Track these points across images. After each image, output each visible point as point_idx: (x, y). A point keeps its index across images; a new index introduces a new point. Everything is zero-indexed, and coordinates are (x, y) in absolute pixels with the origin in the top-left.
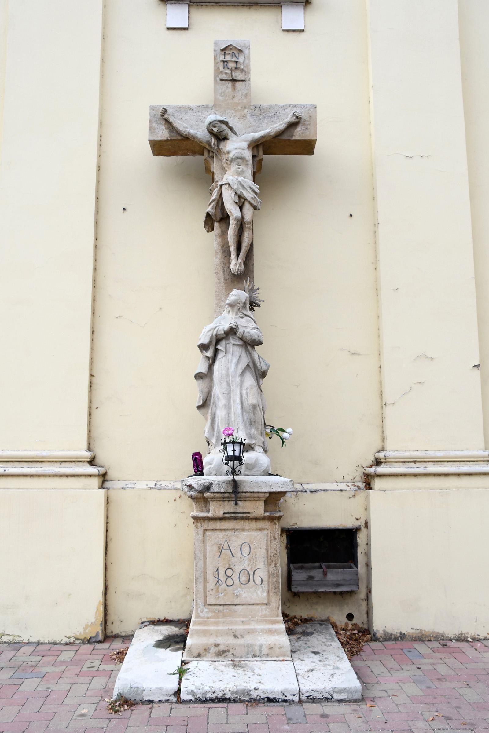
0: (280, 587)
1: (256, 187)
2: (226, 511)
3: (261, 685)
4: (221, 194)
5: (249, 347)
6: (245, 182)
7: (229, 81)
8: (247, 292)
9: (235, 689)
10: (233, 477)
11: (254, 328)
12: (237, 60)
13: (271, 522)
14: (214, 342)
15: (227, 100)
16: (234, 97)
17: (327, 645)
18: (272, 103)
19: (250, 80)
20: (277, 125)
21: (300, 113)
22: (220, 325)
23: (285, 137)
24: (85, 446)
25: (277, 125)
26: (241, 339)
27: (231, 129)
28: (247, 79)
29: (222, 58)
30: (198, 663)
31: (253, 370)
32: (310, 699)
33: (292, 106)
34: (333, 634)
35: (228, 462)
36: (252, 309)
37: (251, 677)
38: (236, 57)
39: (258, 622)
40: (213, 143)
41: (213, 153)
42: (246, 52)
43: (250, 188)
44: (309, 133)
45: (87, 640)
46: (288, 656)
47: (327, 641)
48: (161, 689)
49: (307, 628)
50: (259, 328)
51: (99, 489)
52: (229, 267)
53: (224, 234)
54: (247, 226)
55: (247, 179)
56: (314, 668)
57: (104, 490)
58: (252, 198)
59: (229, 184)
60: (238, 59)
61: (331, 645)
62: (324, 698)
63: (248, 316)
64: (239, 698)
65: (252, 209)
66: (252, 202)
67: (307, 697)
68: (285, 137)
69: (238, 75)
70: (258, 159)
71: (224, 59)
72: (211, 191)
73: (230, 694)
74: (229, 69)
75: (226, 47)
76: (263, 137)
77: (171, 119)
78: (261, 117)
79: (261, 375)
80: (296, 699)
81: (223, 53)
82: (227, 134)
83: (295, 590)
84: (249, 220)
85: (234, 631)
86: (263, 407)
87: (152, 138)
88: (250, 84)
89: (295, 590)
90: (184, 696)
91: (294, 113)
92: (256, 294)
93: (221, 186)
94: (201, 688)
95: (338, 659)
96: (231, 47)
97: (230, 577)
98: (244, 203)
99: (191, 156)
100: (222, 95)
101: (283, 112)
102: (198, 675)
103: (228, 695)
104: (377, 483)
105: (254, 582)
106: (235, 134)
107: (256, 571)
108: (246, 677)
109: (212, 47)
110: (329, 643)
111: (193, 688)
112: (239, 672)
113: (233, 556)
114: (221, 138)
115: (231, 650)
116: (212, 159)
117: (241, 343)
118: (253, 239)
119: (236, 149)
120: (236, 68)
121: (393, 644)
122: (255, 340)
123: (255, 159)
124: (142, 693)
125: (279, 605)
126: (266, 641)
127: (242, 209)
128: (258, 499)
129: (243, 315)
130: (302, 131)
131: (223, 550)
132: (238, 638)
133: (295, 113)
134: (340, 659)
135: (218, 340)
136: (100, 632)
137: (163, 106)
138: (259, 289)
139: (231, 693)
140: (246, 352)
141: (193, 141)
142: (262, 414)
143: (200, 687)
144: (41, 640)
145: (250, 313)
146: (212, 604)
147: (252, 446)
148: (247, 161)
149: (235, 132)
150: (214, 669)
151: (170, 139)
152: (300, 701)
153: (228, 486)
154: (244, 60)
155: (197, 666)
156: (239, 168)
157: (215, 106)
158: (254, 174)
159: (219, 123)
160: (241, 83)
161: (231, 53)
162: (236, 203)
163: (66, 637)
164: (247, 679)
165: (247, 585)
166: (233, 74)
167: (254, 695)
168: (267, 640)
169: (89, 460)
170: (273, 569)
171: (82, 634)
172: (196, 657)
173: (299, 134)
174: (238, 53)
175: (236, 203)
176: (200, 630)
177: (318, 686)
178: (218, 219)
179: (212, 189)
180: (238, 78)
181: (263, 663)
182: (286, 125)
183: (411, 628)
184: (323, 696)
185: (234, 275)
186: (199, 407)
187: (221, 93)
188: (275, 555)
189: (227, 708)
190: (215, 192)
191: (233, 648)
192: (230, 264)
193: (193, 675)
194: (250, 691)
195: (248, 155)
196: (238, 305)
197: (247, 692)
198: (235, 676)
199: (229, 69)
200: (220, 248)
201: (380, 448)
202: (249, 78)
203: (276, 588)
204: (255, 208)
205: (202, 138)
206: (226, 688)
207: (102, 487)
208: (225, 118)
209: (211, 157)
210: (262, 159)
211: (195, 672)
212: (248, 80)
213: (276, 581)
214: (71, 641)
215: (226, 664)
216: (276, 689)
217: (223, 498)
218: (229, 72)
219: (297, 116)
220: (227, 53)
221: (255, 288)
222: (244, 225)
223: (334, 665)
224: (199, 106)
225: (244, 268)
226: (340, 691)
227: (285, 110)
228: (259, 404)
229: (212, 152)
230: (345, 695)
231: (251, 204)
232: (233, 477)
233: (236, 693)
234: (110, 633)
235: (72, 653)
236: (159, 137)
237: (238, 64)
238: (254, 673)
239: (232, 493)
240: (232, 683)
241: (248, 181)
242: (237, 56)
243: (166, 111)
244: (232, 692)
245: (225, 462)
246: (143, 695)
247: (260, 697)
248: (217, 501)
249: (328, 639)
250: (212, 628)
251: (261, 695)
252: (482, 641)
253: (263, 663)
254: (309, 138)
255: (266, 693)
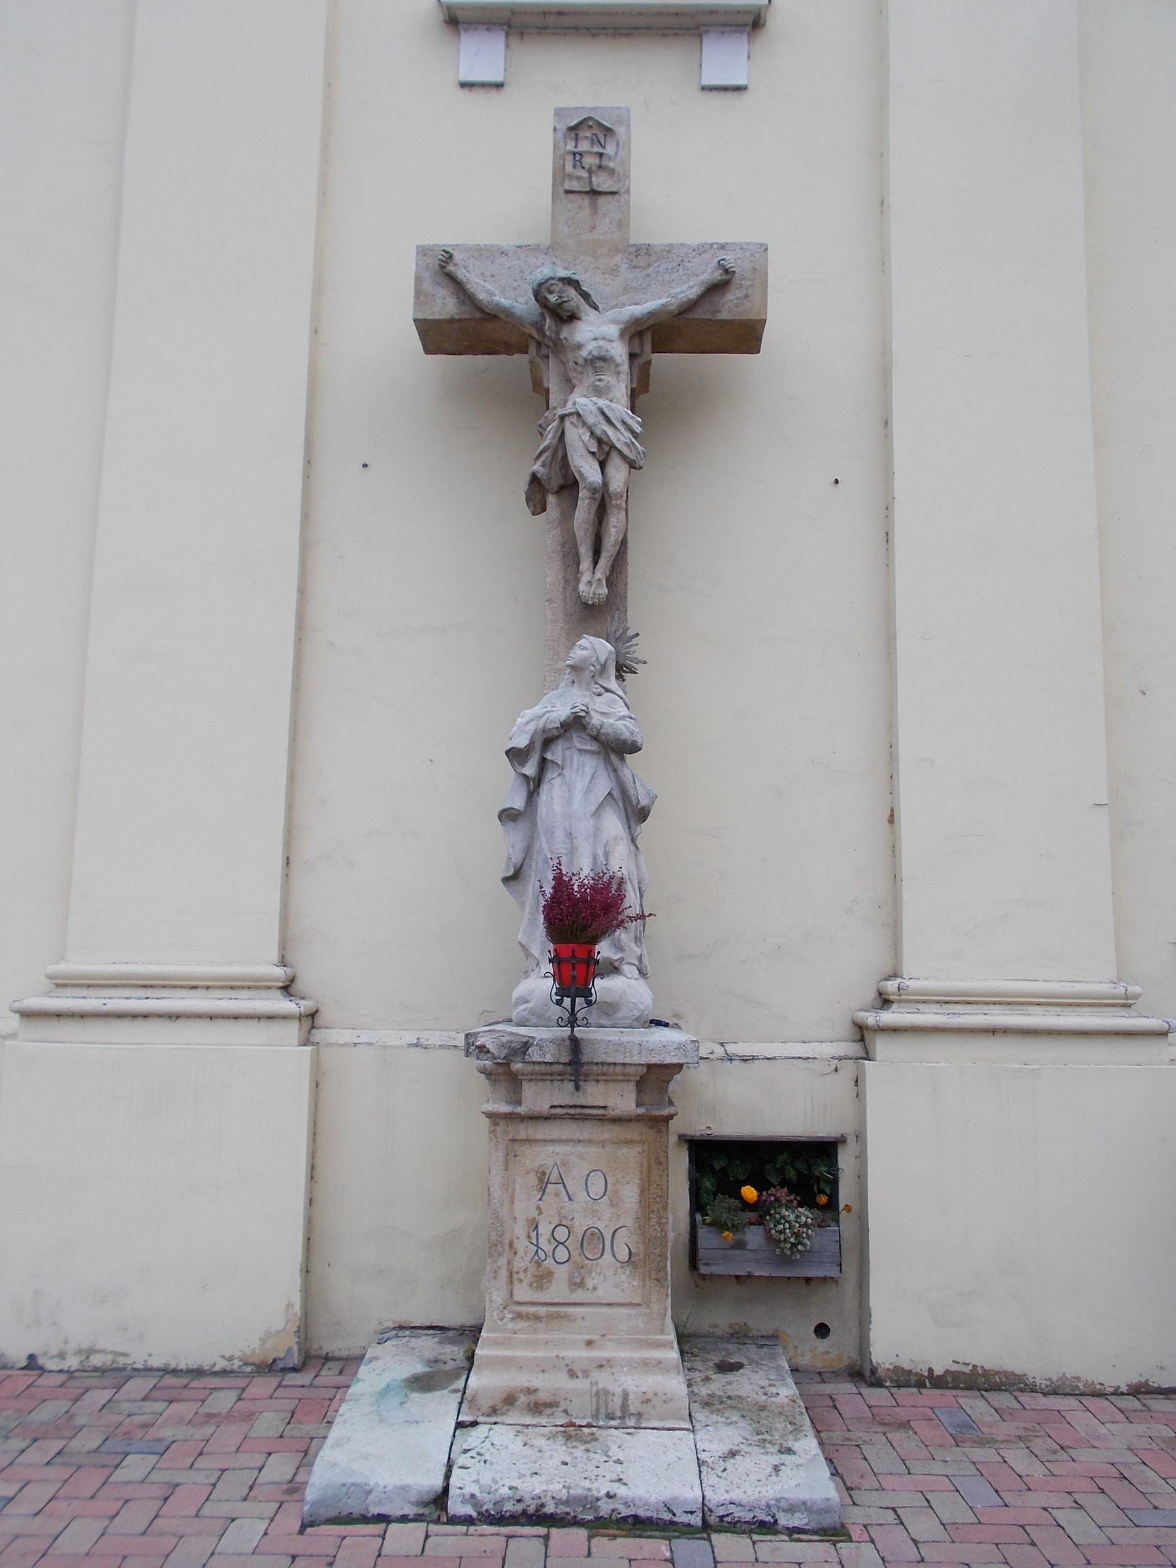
0: (669, 1268)
1: (635, 422)
2: (556, 1103)
3: (622, 1487)
4: (563, 434)
5: (613, 757)
6: (613, 410)
7: (583, 195)
8: (613, 642)
9: (564, 1494)
10: (572, 1031)
11: (623, 718)
12: (601, 150)
13: (652, 1127)
14: (538, 746)
15: (580, 234)
16: (593, 228)
17: (769, 1394)
18: (674, 241)
19: (628, 191)
20: (684, 287)
21: (732, 261)
22: (554, 709)
23: (701, 313)
24: (274, 956)
25: (684, 287)
26: (596, 738)
27: (585, 296)
28: (623, 190)
29: (570, 146)
30: (489, 1430)
31: (621, 806)
32: (727, 1522)
33: (715, 246)
34: (783, 1368)
35: (562, 1000)
36: (620, 677)
37: (602, 1466)
38: (601, 145)
39: (619, 1343)
40: (547, 327)
41: (548, 347)
42: (620, 131)
43: (624, 423)
44: (750, 305)
45: (268, 1365)
46: (684, 1420)
47: (770, 1385)
48: (404, 1489)
49: (730, 1354)
50: (633, 716)
51: (301, 1045)
52: (576, 589)
53: (567, 516)
54: (613, 502)
55: (617, 403)
56: (737, 1448)
57: (310, 1048)
58: (626, 443)
59: (578, 415)
60: (604, 148)
61: (778, 1394)
62: (757, 1521)
63: (613, 692)
64: (572, 1514)
65: (624, 468)
66: (626, 451)
67: (719, 1517)
68: (701, 313)
69: (602, 182)
70: (641, 360)
71: (576, 147)
72: (540, 429)
73: (554, 1506)
74: (583, 168)
75: (580, 123)
76: (651, 314)
77: (461, 274)
78: (649, 272)
79: (636, 814)
80: (696, 1520)
81: (573, 135)
82: (578, 308)
83: (704, 1270)
84: (619, 490)
85: (569, 1362)
86: (639, 883)
87: (420, 316)
88: (628, 201)
89: (704, 1270)
90: (456, 1507)
91: (719, 262)
92: (631, 646)
93: (562, 418)
94: (493, 1489)
95: (790, 1428)
96: (590, 123)
97: (562, 1243)
98: (608, 453)
99: (505, 356)
100: (570, 222)
101: (698, 261)
102: (487, 1457)
103: (550, 1509)
104: (882, 1046)
105: (614, 1256)
106: (595, 307)
107: (618, 1231)
108: (591, 1467)
109: (549, 121)
110: (773, 1390)
111: (475, 1489)
112: (575, 1455)
113: (570, 1199)
114: (565, 317)
115: (562, 1402)
116: (546, 360)
117: (594, 747)
118: (627, 529)
119: (596, 339)
120: (600, 167)
121: (912, 1394)
122: (625, 742)
123: (635, 362)
124: (366, 1499)
125: (666, 1310)
126: (637, 1387)
127: (605, 468)
128: (626, 1078)
129: (600, 689)
130: (735, 301)
131: (549, 1185)
132: (577, 1377)
133: (721, 262)
134: (794, 1430)
135: (548, 740)
136: (295, 1348)
137: (444, 245)
138: (637, 635)
139: (556, 1504)
140: (606, 766)
141: (505, 322)
142: (637, 898)
143: (491, 1487)
144: (171, 1362)
145: (617, 686)
146: (522, 1301)
147: (616, 964)
148: (617, 365)
149: (594, 303)
150: (525, 1445)
151: (458, 317)
152: (706, 1526)
153: (560, 1050)
154: (617, 151)
155: (487, 1437)
156: (600, 380)
157: (552, 250)
158: (634, 395)
159: (560, 284)
160: (610, 197)
161: (589, 135)
162: (593, 453)
163: (223, 1357)
164: (591, 1472)
165: (599, 1261)
166: (594, 179)
167: (605, 1508)
168: (638, 1384)
169: (281, 984)
170: (653, 1228)
171: (257, 1352)
172: (488, 1416)
173: (730, 307)
174: (605, 135)
175: (593, 453)
176: (498, 1357)
177: (745, 1492)
178: (556, 488)
179: (544, 425)
180: (604, 188)
181: (628, 1434)
182: (702, 288)
183: (954, 1361)
184: (754, 1518)
185: (586, 605)
186: (506, 880)
187: (568, 219)
188: (658, 1199)
189: (546, 1538)
190: (550, 431)
191: (565, 1399)
192: (578, 581)
193: (478, 1457)
194: (598, 1499)
195: (619, 351)
196: (592, 668)
197: (590, 1502)
198: (566, 1464)
199: (583, 168)
200: (559, 548)
201: (888, 971)
202: (627, 187)
203: (659, 1271)
204: (632, 465)
205: (525, 315)
206: (546, 1491)
207: (306, 1042)
208: (574, 274)
209: (544, 356)
210: (650, 361)
211: (482, 1451)
212: (625, 192)
213: (660, 1255)
214: (233, 1367)
215: (551, 1432)
216: (653, 1498)
217: (546, 1074)
218: (585, 175)
219: (727, 267)
220: (581, 134)
221: (630, 633)
222: (607, 501)
223: (781, 1444)
224: (520, 247)
225: (607, 591)
226: (792, 1509)
227: (700, 255)
228: (631, 877)
229: (546, 346)
230: (802, 1517)
231: (624, 458)
232: (572, 1031)
233: (567, 1502)
234: (316, 1350)
235: (233, 1395)
236: (437, 314)
237: (604, 158)
238: (608, 1456)
239: (570, 1063)
240: (559, 1480)
241: (619, 407)
242: (602, 141)
243: (451, 257)
244: (558, 1502)
245: (555, 998)
246: (368, 1501)
247: (619, 1513)
248: (537, 1080)
249: (772, 1380)
250: (520, 1353)
251: (620, 1511)
252: (1108, 1397)
253: (628, 1434)
254: (750, 317)
255: (632, 1505)
